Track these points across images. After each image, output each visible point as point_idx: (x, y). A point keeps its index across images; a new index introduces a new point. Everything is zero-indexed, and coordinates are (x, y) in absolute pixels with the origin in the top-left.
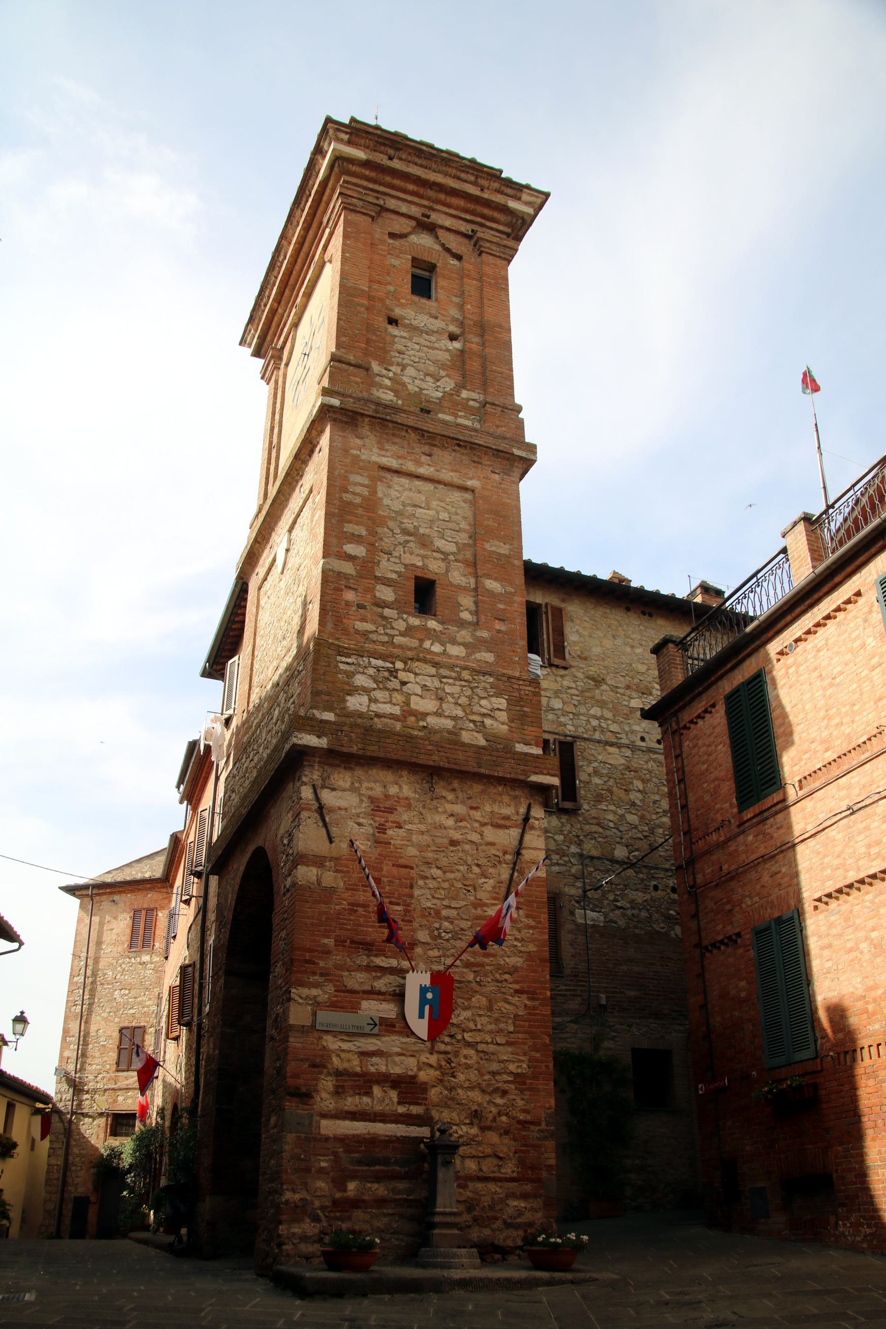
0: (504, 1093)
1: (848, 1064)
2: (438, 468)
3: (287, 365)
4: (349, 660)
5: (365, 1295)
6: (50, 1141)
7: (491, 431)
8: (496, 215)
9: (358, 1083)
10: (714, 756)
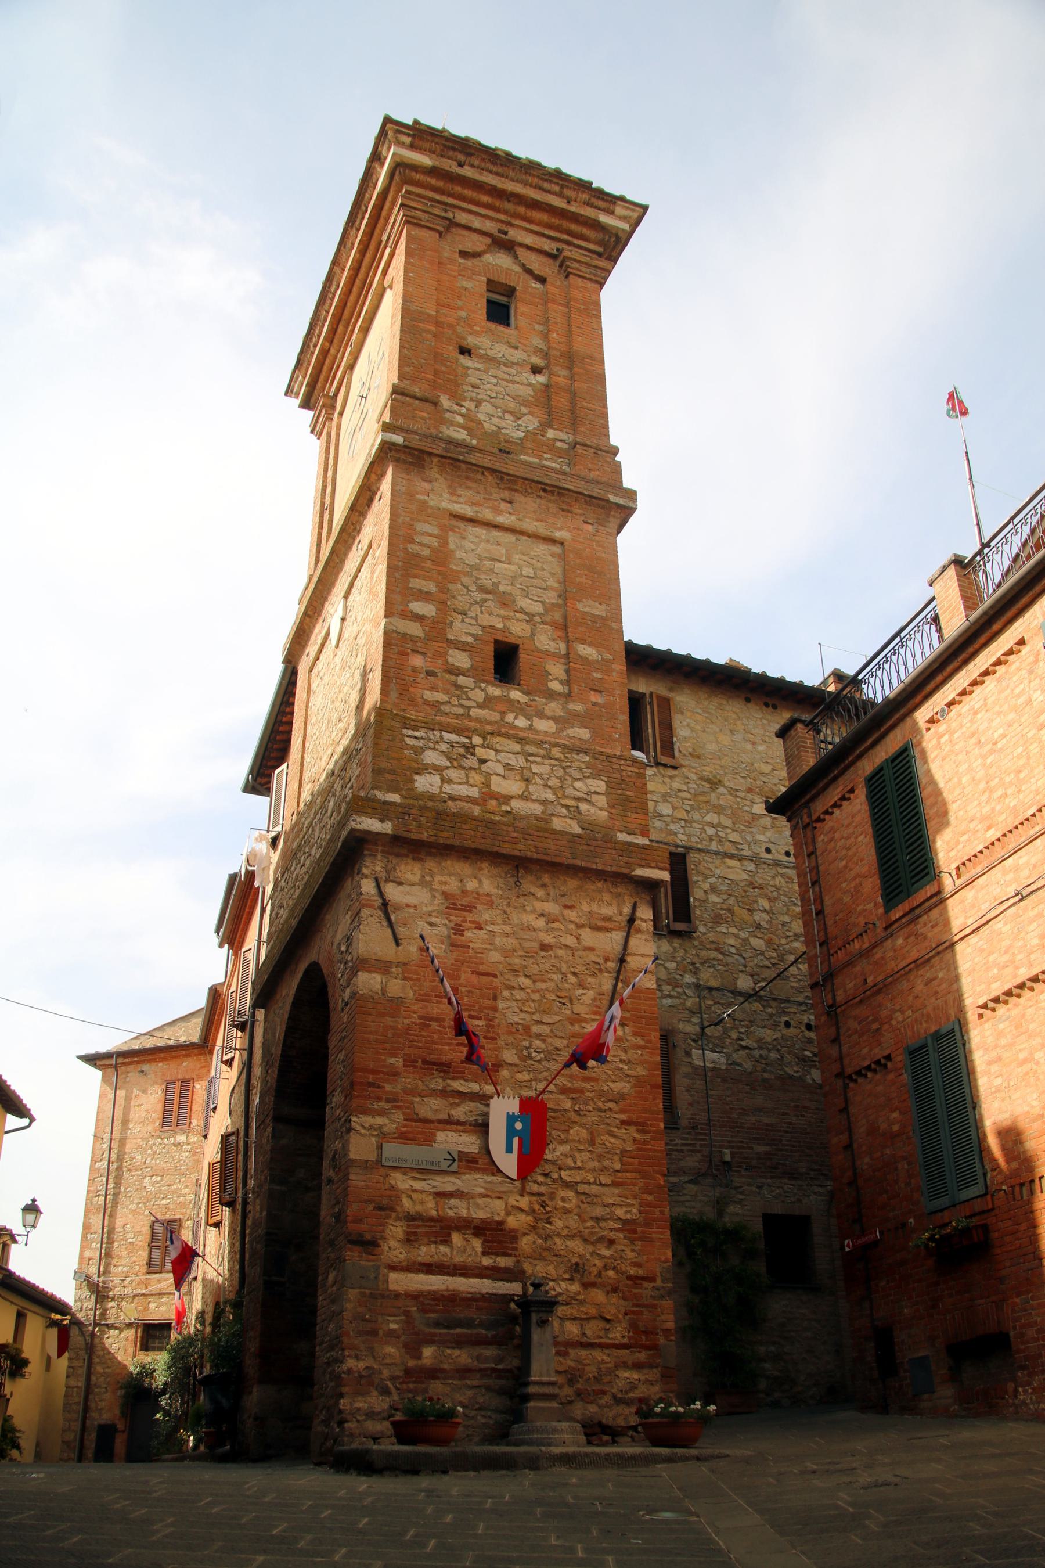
0: (611, 1242)
1: (1025, 1198)
2: (520, 517)
3: (341, 414)
5: (445, 1472)
6: (70, 1359)
7: (583, 474)
8: (585, 231)
9: (434, 1229)
10: (854, 850)
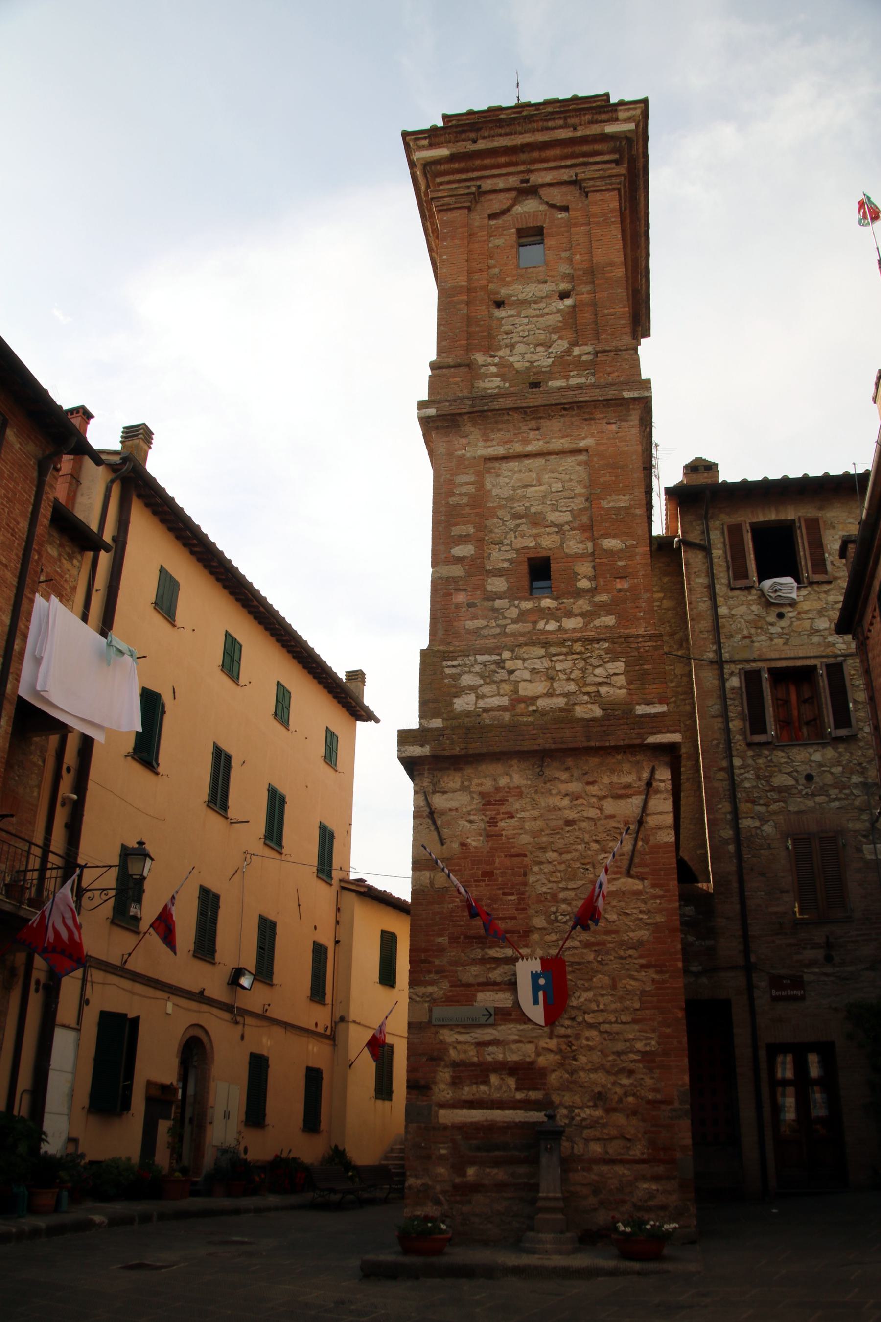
2: (547, 439)
4: (455, 663)
8: (598, 147)
